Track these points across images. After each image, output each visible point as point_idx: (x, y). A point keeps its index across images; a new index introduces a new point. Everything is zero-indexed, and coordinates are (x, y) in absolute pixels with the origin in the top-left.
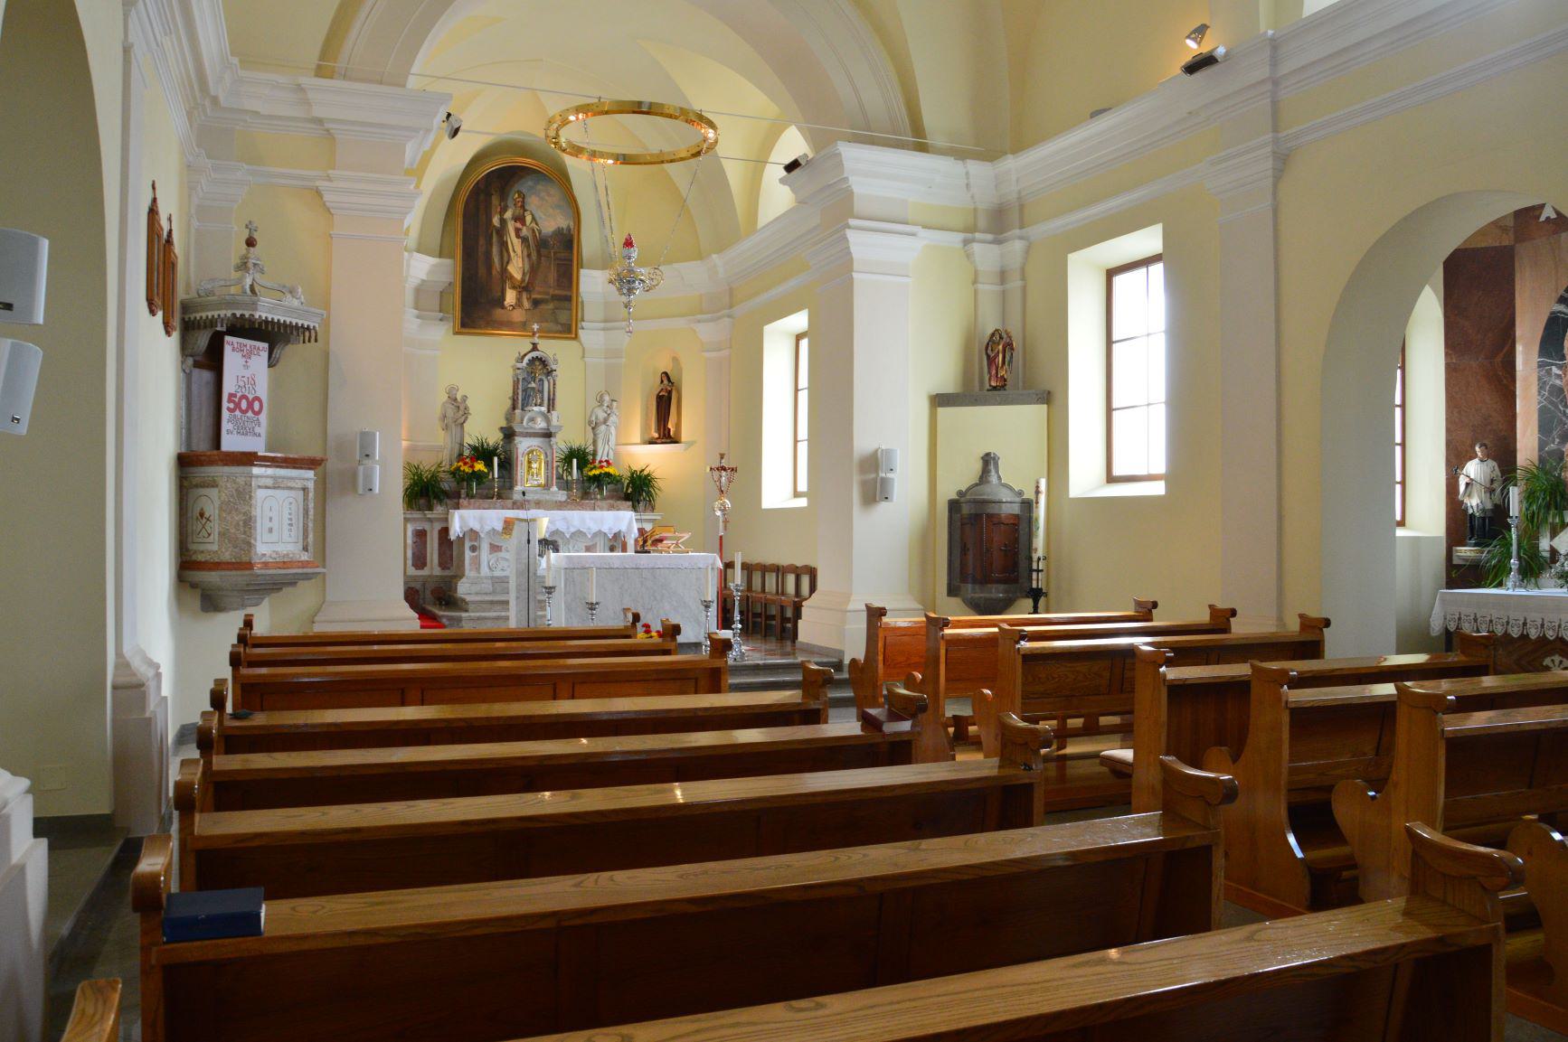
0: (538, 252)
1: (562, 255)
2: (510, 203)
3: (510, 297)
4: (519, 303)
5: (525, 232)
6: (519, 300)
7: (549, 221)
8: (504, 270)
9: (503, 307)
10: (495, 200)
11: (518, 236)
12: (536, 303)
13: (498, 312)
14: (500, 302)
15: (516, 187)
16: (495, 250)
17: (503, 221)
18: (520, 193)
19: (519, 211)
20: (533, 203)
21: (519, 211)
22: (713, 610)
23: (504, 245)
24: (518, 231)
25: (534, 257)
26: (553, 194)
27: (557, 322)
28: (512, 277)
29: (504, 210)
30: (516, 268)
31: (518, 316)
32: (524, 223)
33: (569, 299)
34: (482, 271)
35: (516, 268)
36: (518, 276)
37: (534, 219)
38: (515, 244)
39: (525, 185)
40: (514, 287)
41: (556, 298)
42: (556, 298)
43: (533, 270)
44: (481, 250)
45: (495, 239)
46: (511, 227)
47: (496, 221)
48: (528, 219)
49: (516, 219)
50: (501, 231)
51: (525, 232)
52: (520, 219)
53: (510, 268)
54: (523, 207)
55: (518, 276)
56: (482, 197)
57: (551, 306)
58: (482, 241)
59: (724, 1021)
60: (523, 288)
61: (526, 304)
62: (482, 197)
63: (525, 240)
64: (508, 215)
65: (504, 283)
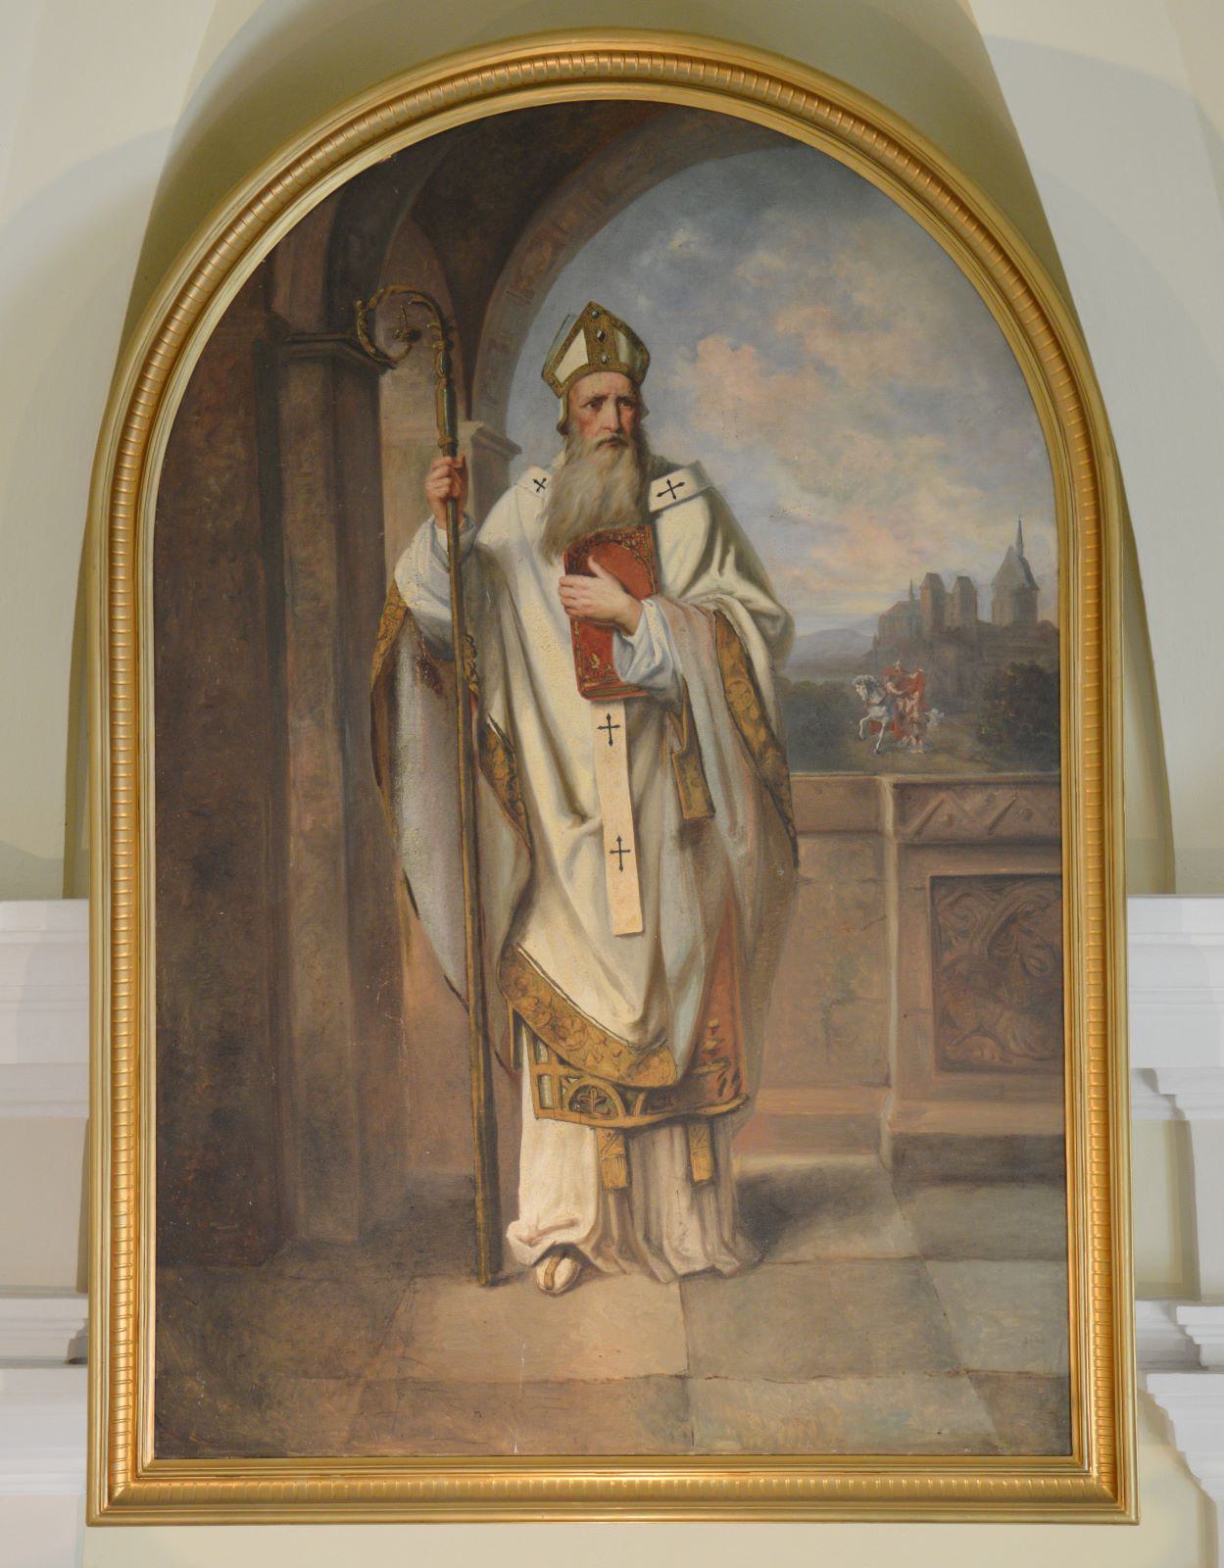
0: (773, 798)
1: (969, 812)
2: (528, 416)
3: (555, 1180)
4: (626, 1228)
5: (654, 642)
6: (624, 1200)
7: (827, 489)
8: (495, 959)
9: (493, 1264)
10: (407, 407)
11: (597, 683)
12: (766, 1217)
13: (458, 1315)
14: (470, 1228)
15: (572, 289)
16: (420, 811)
17: (475, 574)
18: (598, 325)
19: (598, 480)
20: (708, 401)
21: (598, 480)
22: (668, 604)
23: (485, 760)
24: (594, 640)
25: (737, 836)
26: (879, 302)
27: (942, 1361)
28: (559, 1020)
29: (477, 483)
30: (596, 948)
31: (621, 1331)
32: (642, 573)
33: (1039, 1165)
34: (319, 982)
35: (596, 948)
36: (609, 1005)
37: (722, 527)
38: (575, 744)
39: (641, 260)
40: (580, 1103)
41: (922, 1165)
42: (922, 1165)
43: (738, 949)
44: (311, 814)
45: (415, 713)
46: (541, 610)
47: (417, 576)
48: (681, 532)
49: (578, 549)
50: (462, 661)
51: (654, 642)
52: (609, 541)
53: (546, 947)
54: (631, 439)
55: (609, 1005)
56: (301, 393)
57: (893, 1233)
58: (313, 752)
59: (243, 268)
60: (667, 1101)
61: (688, 1233)
62: (301, 393)
63: (656, 710)
64: (515, 519)
65: (495, 1068)
